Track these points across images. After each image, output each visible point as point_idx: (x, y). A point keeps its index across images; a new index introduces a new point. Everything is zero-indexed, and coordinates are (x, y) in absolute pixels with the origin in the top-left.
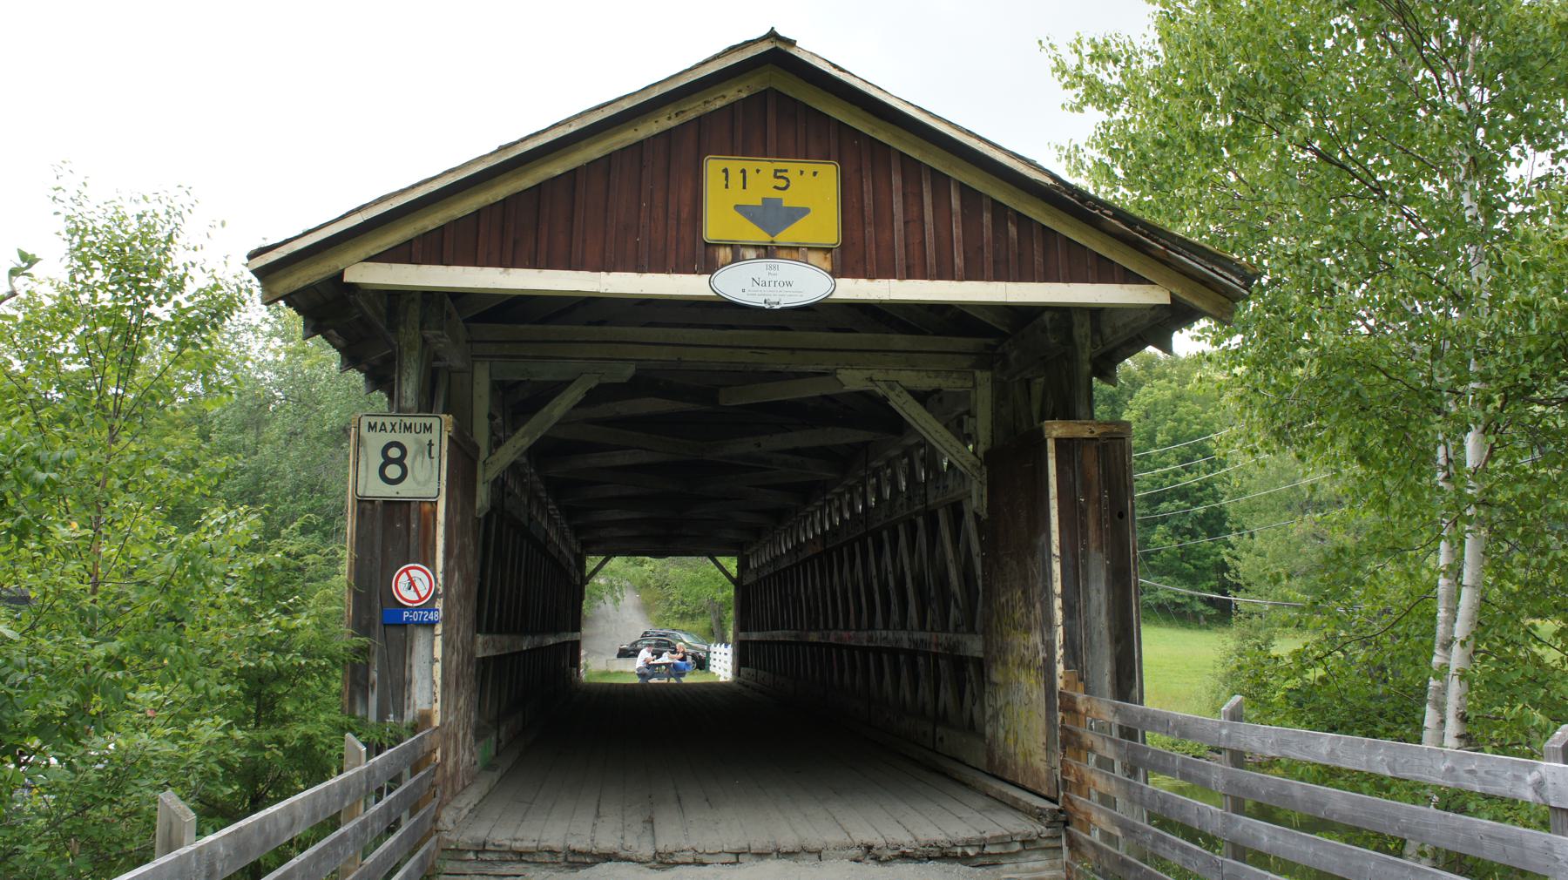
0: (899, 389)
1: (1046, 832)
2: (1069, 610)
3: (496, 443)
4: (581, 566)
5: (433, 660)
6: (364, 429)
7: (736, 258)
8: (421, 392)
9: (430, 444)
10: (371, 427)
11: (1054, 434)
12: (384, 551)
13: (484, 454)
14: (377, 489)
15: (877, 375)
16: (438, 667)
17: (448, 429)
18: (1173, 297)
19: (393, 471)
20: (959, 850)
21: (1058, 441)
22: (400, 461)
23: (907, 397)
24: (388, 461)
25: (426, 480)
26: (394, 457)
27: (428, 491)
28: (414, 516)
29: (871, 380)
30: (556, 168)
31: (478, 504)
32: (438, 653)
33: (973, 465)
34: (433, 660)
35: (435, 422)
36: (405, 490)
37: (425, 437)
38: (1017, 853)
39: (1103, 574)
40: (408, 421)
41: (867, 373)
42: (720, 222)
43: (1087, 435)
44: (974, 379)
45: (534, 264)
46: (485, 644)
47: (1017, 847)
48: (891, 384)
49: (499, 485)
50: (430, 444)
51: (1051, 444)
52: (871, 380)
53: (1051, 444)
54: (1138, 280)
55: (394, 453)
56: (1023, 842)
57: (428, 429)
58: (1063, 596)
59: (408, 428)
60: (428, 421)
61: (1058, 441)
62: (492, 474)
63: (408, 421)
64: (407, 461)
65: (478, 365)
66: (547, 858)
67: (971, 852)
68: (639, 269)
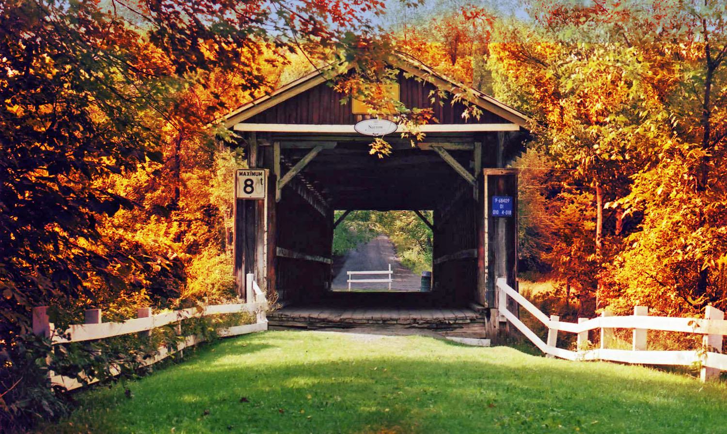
0: (443, 150)
1: (480, 317)
2: (491, 238)
3: (282, 177)
4: (332, 216)
5: (264, 253)
6: (238, 174)
7: (364, 119)
8: (258, 160)
9: (261, 180)
10: (241, 174)
11: (488, 173)
12: (246, 216)
13: (278, 178)
14: (243, 195)
15: (434, 144)
16: (265, 256)
17: (267, 174)
18: (520, 127)
19: (249, 189)
20: (447, 322)
21: (489, 176)
22: (251, 186)
23: (446, 153)
24: (247, 185)
25: (260, 192)
26: (249, 184)
27: (261, 196)
28: (256, 204)
29: (431, 146)
30: (302, 89)
31: (277, 198)
32: (266, 251)
33: (473, 181)
34: (264, 253)
35: (263, 172)
36: (253, 196)
37: (260, 177)
38: (468, 323)
39: (504, 225)
40: (253, 171)
41: (430, 144)
42: (357, 107)
43: (500, 174)
44: (474, 146)
45: (297, 122)
46: (280, 251)
47: (468, 321)
48: (439, 148)
49: (283, 190)
50: (261, 180)
51: (486, 178)
52: (431, 146)
53: (486, 178)
54: (508, 122)
55: (249, 183)
56: (471, 320)
57: (260, 174)
58: (489, 233)
59: (253, 174)
60: (260, 171)
61: (489, 176)
62: (282, 185)
63: (253, 171)
64: (254, 185)
65: (275, 143)
66: (303, 320)
67: (451, 322)
68: (331, 123)
